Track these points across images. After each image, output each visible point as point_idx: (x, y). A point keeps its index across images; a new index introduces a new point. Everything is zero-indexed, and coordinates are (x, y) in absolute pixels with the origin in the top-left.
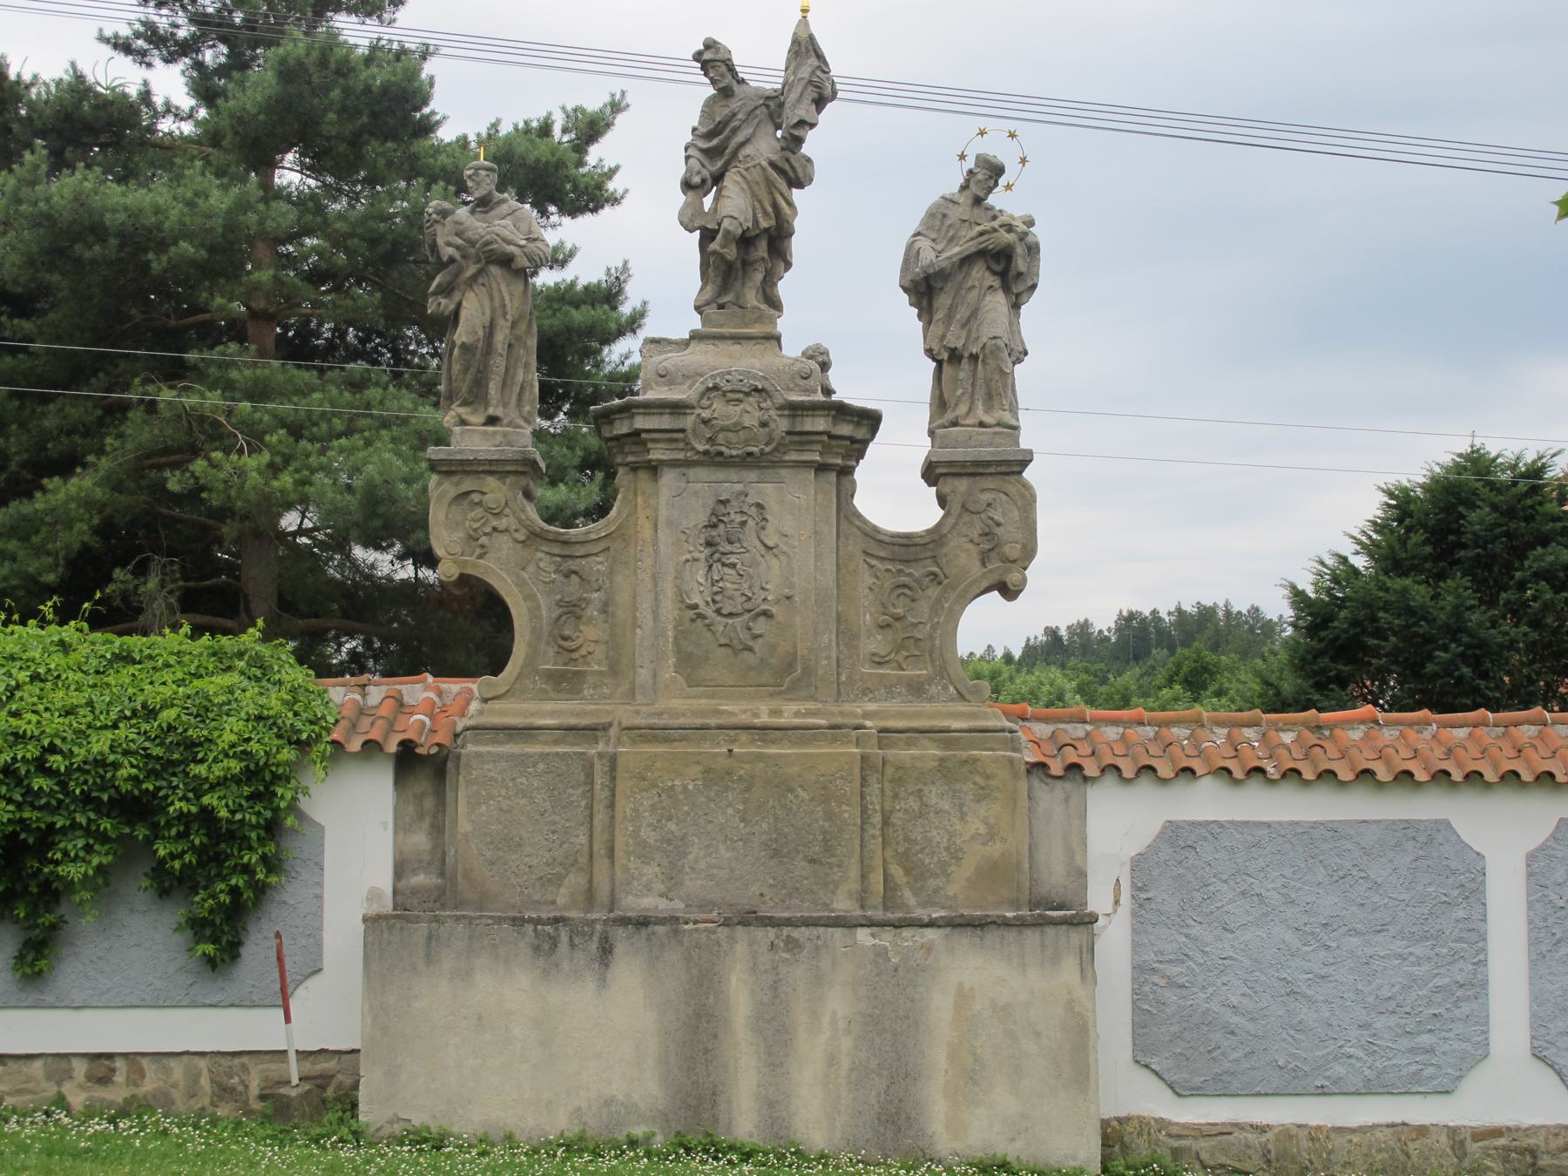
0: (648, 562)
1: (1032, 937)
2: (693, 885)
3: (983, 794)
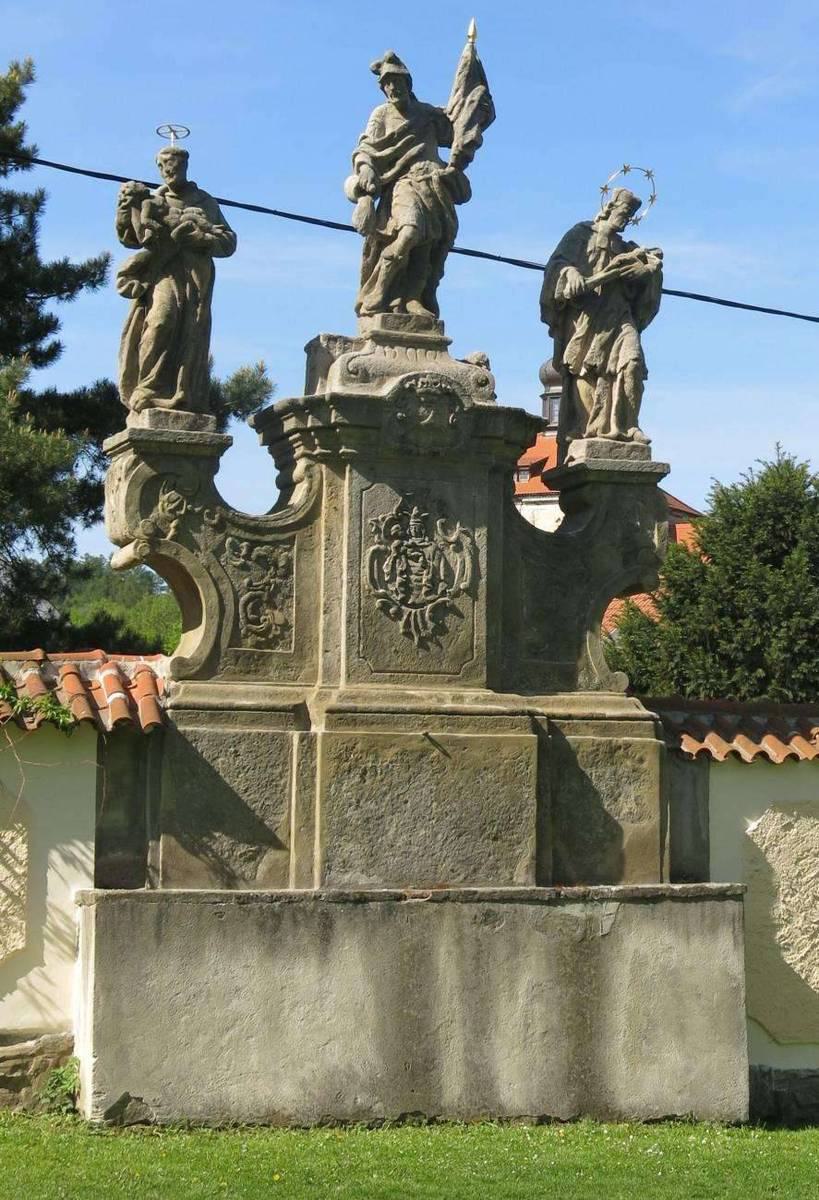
1: (693, 908)
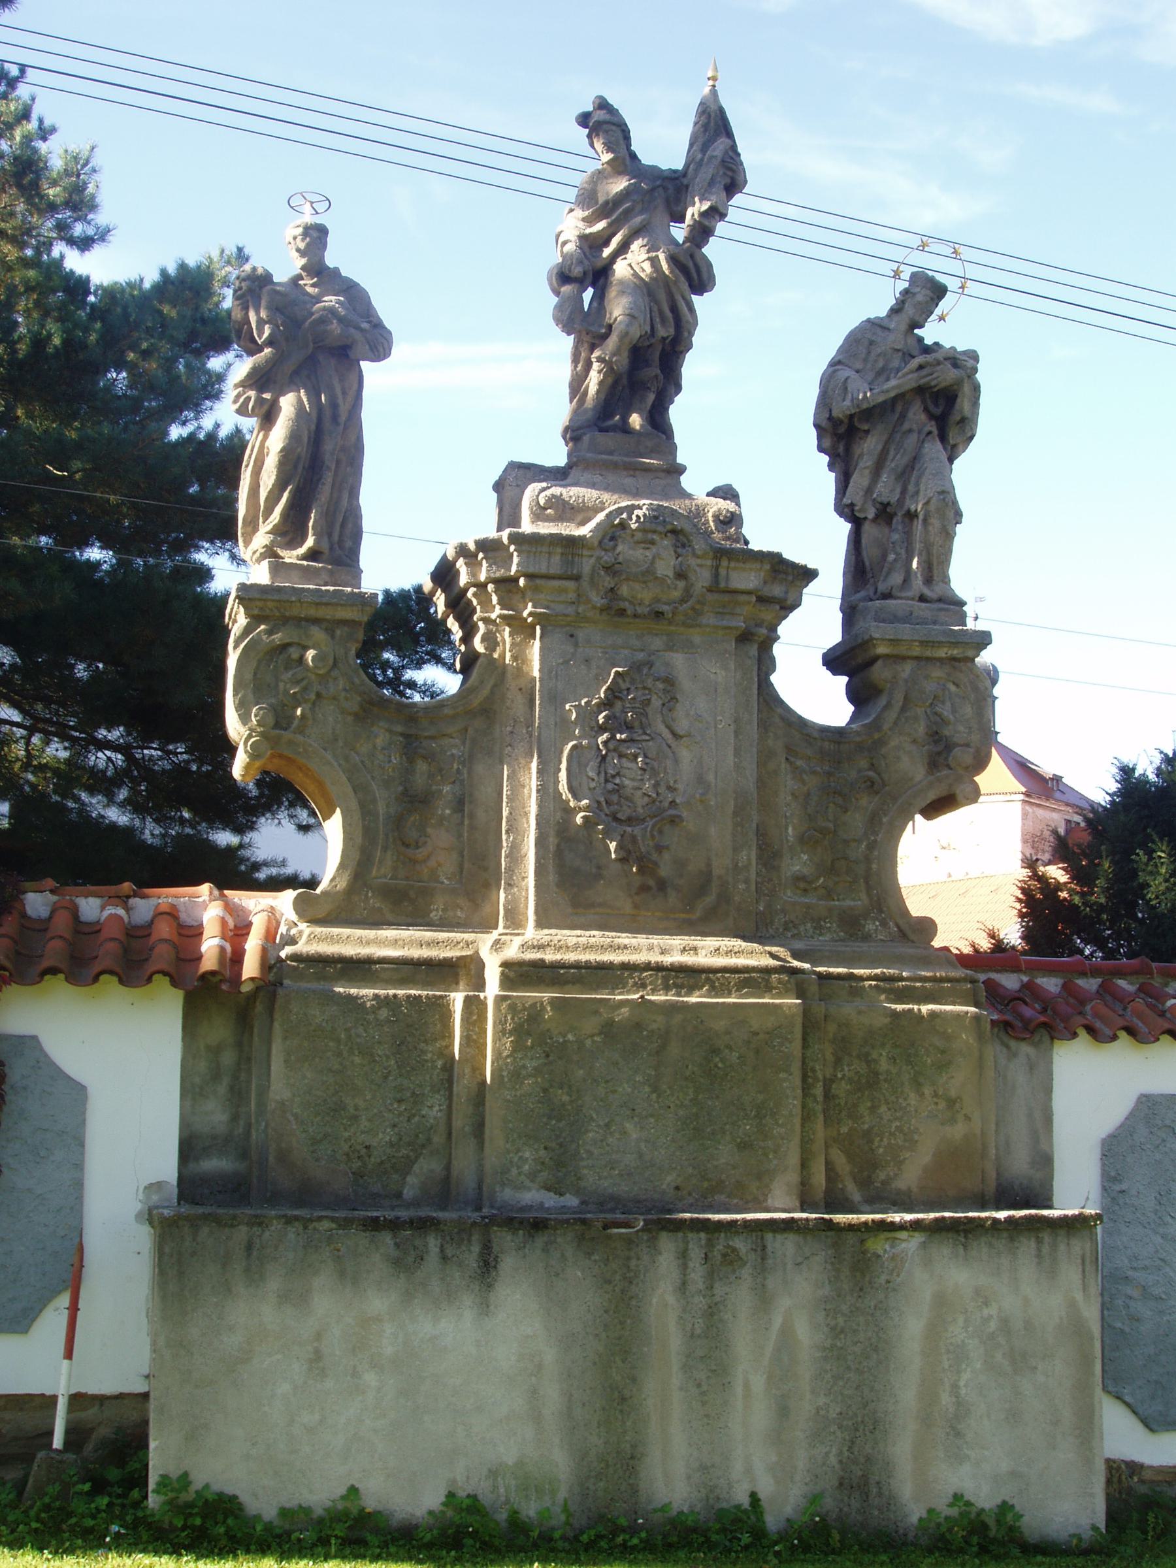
1: (1027, 1246)
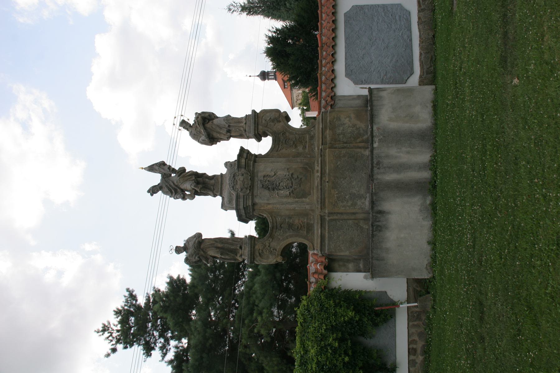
0: (278, 206)
1: (375, 103)
2: (362, 192)
3: (339, 119)
